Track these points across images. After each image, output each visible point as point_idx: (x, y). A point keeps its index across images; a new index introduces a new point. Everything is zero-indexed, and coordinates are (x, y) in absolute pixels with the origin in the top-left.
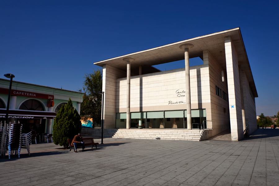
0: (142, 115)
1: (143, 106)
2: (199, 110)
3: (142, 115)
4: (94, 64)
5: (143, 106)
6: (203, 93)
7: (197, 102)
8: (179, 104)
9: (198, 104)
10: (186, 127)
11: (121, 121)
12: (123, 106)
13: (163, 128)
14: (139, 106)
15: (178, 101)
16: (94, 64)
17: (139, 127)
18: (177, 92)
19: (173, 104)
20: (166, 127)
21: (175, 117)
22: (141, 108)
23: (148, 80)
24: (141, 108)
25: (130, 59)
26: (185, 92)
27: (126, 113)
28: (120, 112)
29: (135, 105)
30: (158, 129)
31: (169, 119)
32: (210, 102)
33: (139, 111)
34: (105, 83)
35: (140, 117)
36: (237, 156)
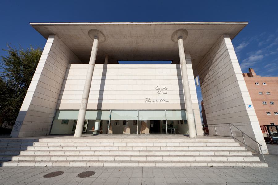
0: (99, 115)
1: (103, 102)
2: (97, 111)
3: (99, 115)
4: (30, 24)
5: (103, 102)
6: (98, 93)
7: (96, 102)
8: (159, 102)
9: (98, 103)
10: (166, 134)
11: (62, 123)
12: (67, 101)
13: (149, 133)
14: (179, 102)
15: (159, 99)
16: (30, 24)
17: (95, 133)
18: (157, 88)
19: (151, 102)
20: (133, 132)
21: (132, 119)
22: (100, 104)
23: (111, 67)
24: (100, 104)
25: (100, 34)
26: (167, 89)
27: (79, 110)
28: (102, 109)
29: (93, 102)
30: (121, 134)
31: (117, 122)
32: (197, 102)
33: (96, 109)
34: (46, 58)
35: (95, 118)
36: (8, 149)
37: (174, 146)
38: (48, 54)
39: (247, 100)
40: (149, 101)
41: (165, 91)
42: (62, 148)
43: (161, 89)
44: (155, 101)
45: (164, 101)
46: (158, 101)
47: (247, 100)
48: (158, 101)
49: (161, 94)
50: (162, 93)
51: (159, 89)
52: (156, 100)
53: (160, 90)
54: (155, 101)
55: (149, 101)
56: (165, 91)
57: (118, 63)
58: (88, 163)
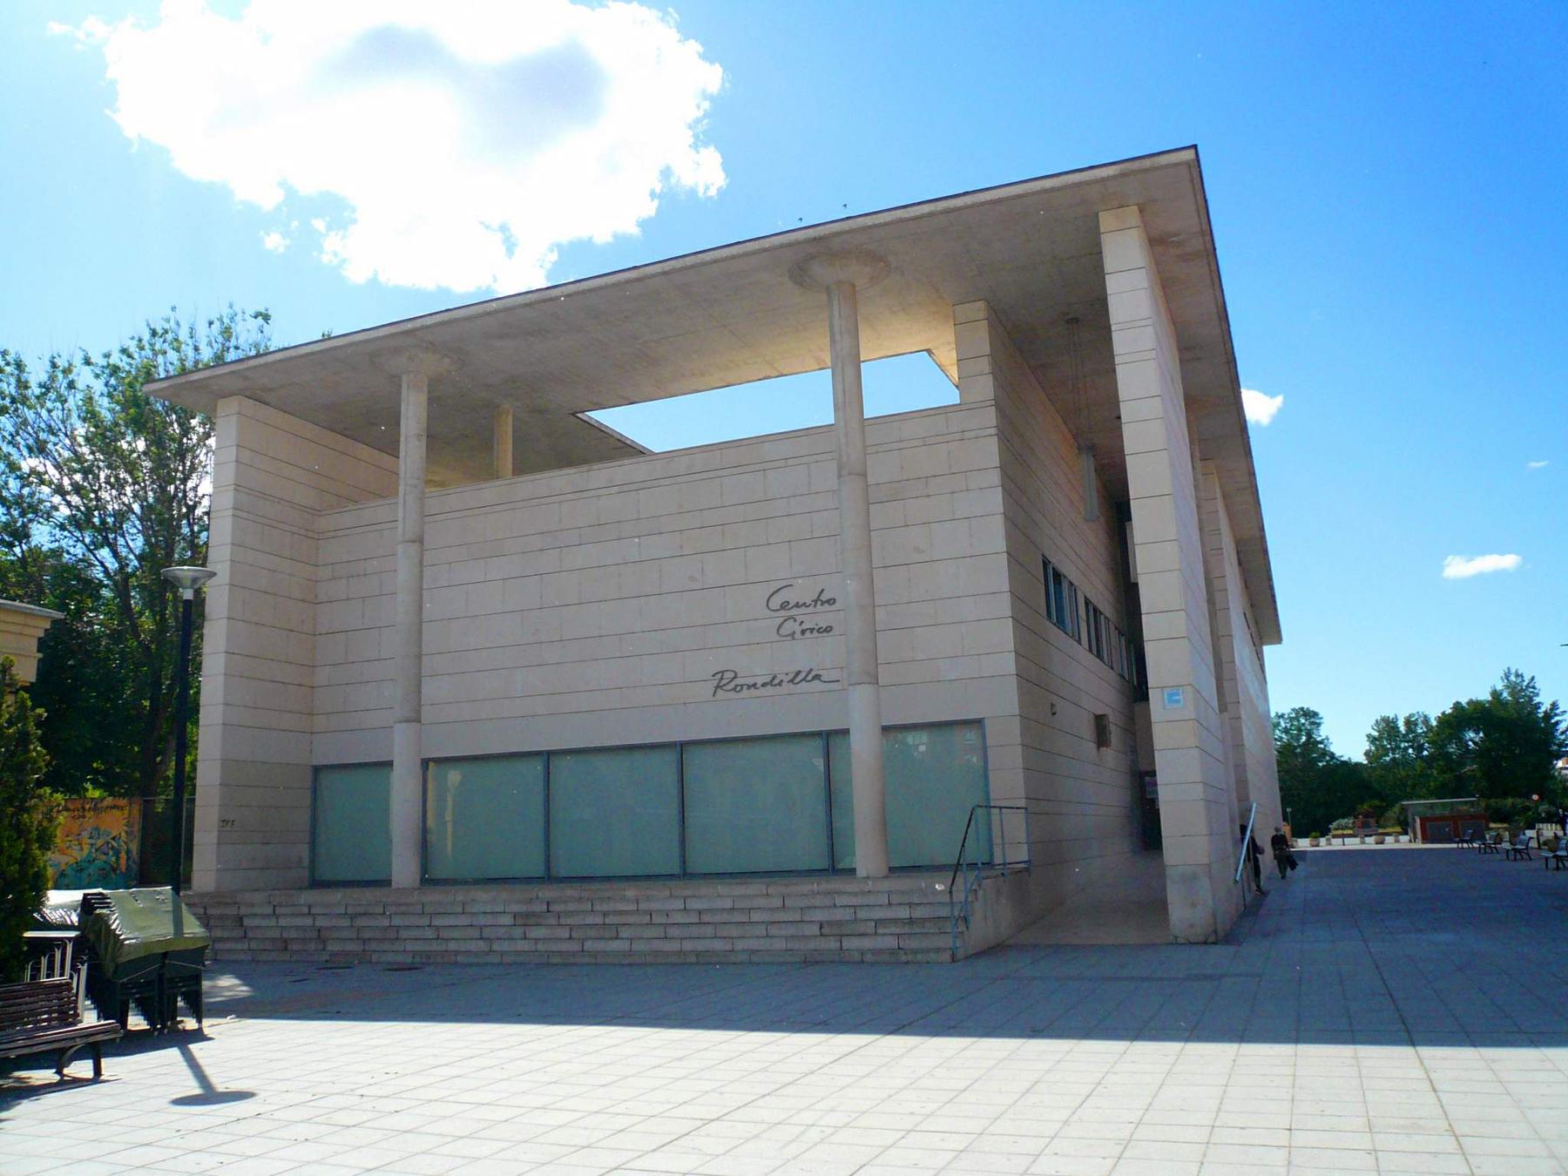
18: (776, 602)
26: (831, 601)
37: (910, 905)
38: (230, 512)
39: (1353, 844)
40: (732, 685)
41: (823, 617)
42: (548, 868)
43: (797, 605)
44: (764, 685)
45: (817, 677)
46: (780, 684)
47: (1353, 844)
48: (780, 684)
49: (798, 635)
50: (803, 632)
51: (784, 606)
52: (768, 679)
53: (794, 612)
54: (764, 685)
55: (732, 685)
56: (823, 617)
57: (1136, 585)
58: (1196, 752)
